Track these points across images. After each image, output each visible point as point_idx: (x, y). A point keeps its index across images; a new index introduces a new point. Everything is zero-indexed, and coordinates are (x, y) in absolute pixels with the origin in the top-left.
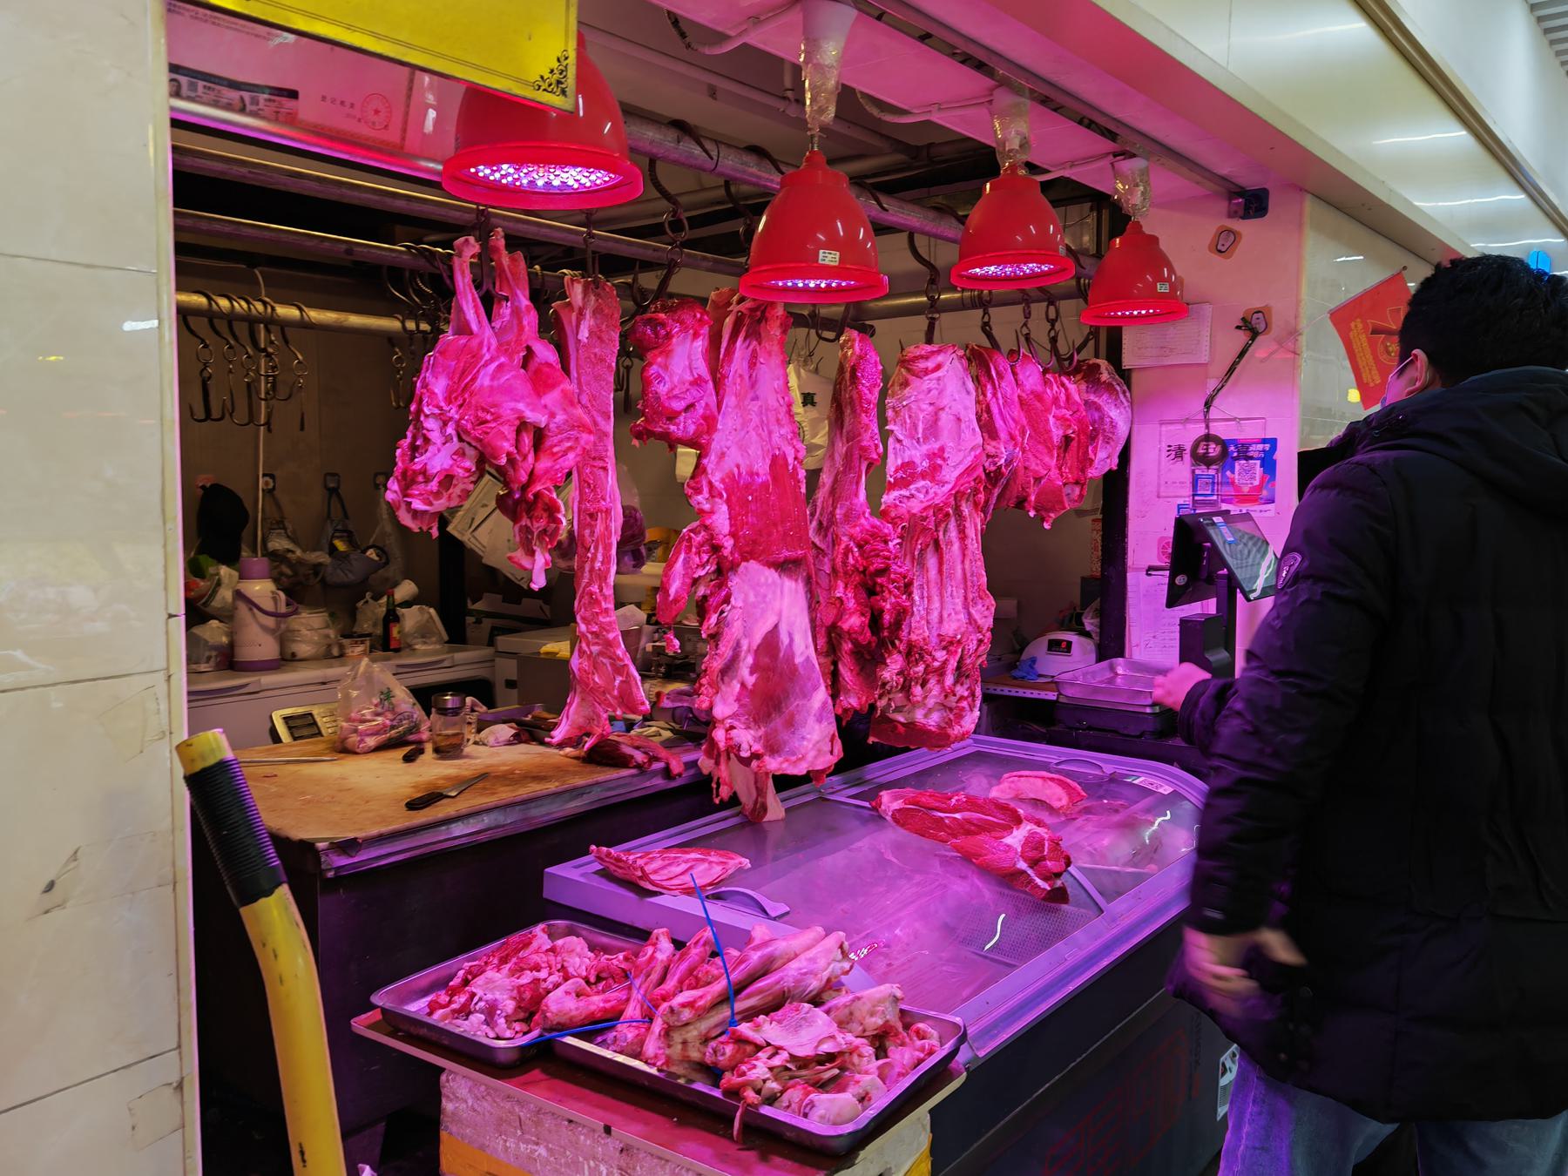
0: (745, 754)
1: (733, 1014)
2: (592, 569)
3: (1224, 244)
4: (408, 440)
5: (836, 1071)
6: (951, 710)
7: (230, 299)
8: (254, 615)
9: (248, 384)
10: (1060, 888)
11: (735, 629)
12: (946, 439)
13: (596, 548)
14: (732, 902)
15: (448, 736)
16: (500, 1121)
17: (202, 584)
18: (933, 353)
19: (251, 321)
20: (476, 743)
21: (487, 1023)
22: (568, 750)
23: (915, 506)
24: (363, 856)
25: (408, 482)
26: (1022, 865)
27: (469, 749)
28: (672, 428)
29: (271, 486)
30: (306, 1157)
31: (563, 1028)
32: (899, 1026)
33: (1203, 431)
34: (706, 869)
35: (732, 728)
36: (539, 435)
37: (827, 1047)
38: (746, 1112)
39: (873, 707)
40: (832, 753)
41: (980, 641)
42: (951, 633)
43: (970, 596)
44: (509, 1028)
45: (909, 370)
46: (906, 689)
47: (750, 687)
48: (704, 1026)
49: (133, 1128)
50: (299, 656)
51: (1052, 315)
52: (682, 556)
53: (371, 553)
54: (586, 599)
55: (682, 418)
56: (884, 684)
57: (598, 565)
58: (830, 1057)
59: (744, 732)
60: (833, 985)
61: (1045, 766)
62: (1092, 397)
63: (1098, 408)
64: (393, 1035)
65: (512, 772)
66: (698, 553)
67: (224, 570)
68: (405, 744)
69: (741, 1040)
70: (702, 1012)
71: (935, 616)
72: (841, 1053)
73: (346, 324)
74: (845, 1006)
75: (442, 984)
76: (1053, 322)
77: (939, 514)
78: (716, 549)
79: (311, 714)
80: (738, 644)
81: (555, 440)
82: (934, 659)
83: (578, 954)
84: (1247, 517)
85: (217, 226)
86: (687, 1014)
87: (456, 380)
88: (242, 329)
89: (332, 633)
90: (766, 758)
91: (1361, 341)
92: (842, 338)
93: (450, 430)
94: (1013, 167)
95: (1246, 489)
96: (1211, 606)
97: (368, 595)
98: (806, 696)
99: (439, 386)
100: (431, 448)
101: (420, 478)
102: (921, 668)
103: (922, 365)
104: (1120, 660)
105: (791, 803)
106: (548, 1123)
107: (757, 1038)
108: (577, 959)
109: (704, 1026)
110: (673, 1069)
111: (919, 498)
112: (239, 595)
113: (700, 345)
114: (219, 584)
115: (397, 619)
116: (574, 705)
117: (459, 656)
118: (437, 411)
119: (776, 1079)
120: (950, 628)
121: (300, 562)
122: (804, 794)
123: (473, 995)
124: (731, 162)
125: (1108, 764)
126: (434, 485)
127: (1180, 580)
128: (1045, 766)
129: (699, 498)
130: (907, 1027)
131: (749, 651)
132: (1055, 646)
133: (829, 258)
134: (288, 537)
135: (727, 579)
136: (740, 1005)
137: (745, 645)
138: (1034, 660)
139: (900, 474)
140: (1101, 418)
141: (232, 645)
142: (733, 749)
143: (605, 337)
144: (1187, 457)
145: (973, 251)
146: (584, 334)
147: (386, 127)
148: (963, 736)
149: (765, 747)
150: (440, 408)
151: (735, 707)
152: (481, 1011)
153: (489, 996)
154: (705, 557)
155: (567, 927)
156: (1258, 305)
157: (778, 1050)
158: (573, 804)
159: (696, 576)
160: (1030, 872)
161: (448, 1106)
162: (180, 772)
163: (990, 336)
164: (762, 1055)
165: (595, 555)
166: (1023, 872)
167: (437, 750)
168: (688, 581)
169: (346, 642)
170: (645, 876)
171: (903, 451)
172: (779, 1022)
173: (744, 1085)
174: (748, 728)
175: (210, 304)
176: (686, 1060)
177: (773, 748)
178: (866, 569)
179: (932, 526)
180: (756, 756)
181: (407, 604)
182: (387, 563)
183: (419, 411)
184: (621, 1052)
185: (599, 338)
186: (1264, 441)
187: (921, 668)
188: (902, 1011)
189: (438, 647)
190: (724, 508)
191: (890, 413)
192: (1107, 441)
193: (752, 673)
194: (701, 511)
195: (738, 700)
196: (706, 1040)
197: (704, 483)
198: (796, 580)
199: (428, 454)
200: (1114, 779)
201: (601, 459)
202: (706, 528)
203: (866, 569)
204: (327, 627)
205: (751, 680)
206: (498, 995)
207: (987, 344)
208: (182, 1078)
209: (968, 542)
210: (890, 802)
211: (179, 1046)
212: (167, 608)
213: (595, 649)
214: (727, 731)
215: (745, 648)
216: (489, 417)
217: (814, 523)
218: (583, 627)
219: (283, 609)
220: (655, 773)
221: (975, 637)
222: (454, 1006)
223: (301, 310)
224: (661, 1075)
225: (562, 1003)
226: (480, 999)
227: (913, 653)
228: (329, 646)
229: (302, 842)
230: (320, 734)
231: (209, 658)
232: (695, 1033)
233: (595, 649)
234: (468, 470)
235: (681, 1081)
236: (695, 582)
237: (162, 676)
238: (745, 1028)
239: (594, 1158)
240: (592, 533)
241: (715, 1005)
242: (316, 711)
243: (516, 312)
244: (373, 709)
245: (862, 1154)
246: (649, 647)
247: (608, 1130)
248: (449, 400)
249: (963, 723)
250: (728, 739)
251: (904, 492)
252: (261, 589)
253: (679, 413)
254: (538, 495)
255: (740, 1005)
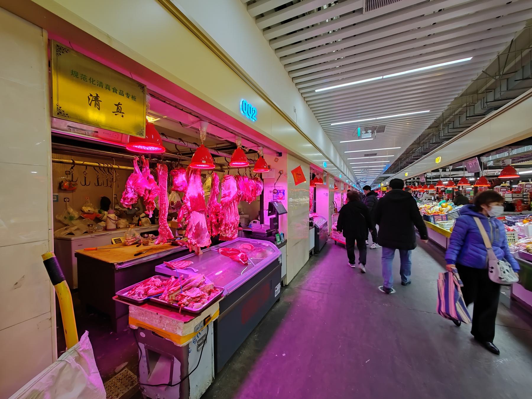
0: (193, 244)
1: (182, 291)
2: (162, 214)
3: (276, 160)
4: (125, 192)
5: (200, 299)
6: (233, 234)
7: (103, 164)
8: (110, 220)
9: (107, 179)
10: (246, 263)
11: (192, 223)
12: (231, 190)
13: (163, 210)
14: (189, 270)
15: (145, 242)
16: (139, 314)
17: (101, 215)
18: (229, 176)
19: (108, 168)
20: (151, 242)
21: (138, 296)
22: (169, 243)
23: (226, 201)
24: (124, 265)
25: (124, 199)
26: (240, 260)
27: (150, 244)
28: (178, 189)
29: (116, 197)
30: (67, 332)
31: (151, 296)
32: (214, 289)
33: (274, 189)
34: (185, 264)
35: (191, 239)
36: (150, 192)
37: (198, 295)
38: (182, 308)
39: (219, 235)
40: (209, 243)
41: (237, 223)
42: (232, 222)
43: (236, 215)
44: (143, 296)
45: (225, 179)
46: (225, 231)
47: (194, 232)
48: (176, 294)
49: (38, 328)
50: (120, 228)
51: (250, 170)
52: (182, 211)
53: (136, 209)
54: (161, 219)
55: (180, 187)
56: (221, 230)
57: (163, 213)
58: (199, 297)
59: (193, 240)
60: (201, 284)
61: (249, 242)
62: (257, 183)
63: (258, 185)
64: (120, 300)
65: (157, 248)
66: (185, 210)
67: (106, 212)
68: (137, 243)
69: (182, 295)
70: (175, 291)
71: (230, 219)
72: (201, 296)
73: (127, 169)
74: (203, 287)
75: (131, 289)
76: (250, 171)
77: (230, 202)
78: (188, 209)
79: (120, 239)
80: (192, 225)
81: (153, 192)
82: (230, 226)
83: (158, 282)
84: (281, 202)
85: (95, 152)
86: (172, 292)
87: (134, 181)
88: (106, 170)
89: (127, 223)
90: (197, 244)
91: (295, 175)
92: (212, 174)
93: (133, 190)
94: (239, 148)
95: (281, 197)
96: (274, 216)
97: (135, 216)
98: (205, 233)
99: (131, 183)
100: (129, 193)
101: (127, 199)
102: (227, 227)
103: (227, 178)
104: (263, 224)
105: (204, 252)
106: (148, 313)
107: (185, 295)
108: (158, 283)
109: (176, 294)
110: (170, 302)
111: (227, 199)
112: (107, 217)
113: (184, 175)
114: (104, 215)
115: (141, 220)
116: (159, 237)
117: (152, 227)
118: (130, 187)
119: (188, 301)
120: (232, 221)
121: (121, 210)
122: (205, 250)
123: (135, 291)
124: (190, 145)
125: (259, 241)
126: (129, 200)
127: (270, 212)
128: (249, 242)
129: (185, 200)
130: (215, 289)
131: (194, 226)
132: (254, 222)
133: (204, 162)
134: (119, 206)
135: (190, 214)
136: (183, 289)
137: (193, 225)
138: (251, 225)
139: (224, 196)
140: (259, 186)
141: (106, 226)
142: (191, 243)
143: (164, 174)
144: (272, 192)
145: (233, 160)
146: (161, 173)
147: (118, 138)
148: (235, 239)
149: (197, 243)
150: (131, 186)
151: (192, 236)
152: (137, 294)
153: (139, 291)
154: (186, 211)
155: (159, 276)
156: (281, 170)
157: (189, 296)
158: (169, 253)
159: (184, 214)
160: (242, 261)
161: (130, 312)
162: (42, 261)
163: (239, 173)
164: (186, 298)
165: (163, 211)
166: (241, 261)
167: (143, 244)
168: (183, 215)
169: (130, 225)
170: (173, 267)
171: (224, 192)
172: (190, 291)
173: (182, 304)
174: (194, 239)
175: (99, 165)
176: (172, 300)
177: (198, 243)
178: (216, 212)
179: (229, 204)
180: (195, 244)
181: (143, 217)
182: (139, 210)
183: (127, 187)
184: (162, 300)
185: (163, 174)
186: (283, 190)
187: (227, 227)
188: (214, 287)
189: (149, 225)
190: (189, 202)
191: (222, 186)
192: (260, 190)
193: (195, 230)
194: (185, 203)
195: (192, 235)
196: (176, 296)
197: (186, 198)
198: (203, 214)
199: (128, 194)
200: (260, 244)
201: (164, 195)
202: (186, 206)
203: (216, 212)
204: (126, 222)
205: (194, 231)
206: (141, 291)
207: (239, 175)
208: (51, 317)
209: (235, 207)
210: (220, 250)
211: (51, 311)
212: (48, 228)
213: (163, 227)
214: (190, 240)
215: (193, 226)
216: (139, 188)
217: (208, 204)
218: (160, 224)
219: (117, 219)
220: (184, 247)
221: (237, 222)
222: (132, 293)
223: (118, 166)
224: (168, 303)
225: (152, 291)
226: (137, 292)
227: (226, 225)
228: (127, 226)
229: (111, 263)
230: (121, 242)
231: (101, 229)
232: (174, 295)
233: (163, 227)
234: (136, 197)
235: (171, 304)
236: (184, 215)
237: (47, 241)
238: (183, 293)
239: (155, 319)
240: (162, 207)
241: (178, 290)
242: (121, 238)
243: (146, 170)
244: (131, 237)
245: (202, 313)
246: (185, 225)
247: (157, 314)
248: (132, 185)
249: (235, 236)
250: (191, 241)
251: (224, 198)
252: (112, 216)
253: (180, 187)
254: (150, 201)
255: (183, 289)
